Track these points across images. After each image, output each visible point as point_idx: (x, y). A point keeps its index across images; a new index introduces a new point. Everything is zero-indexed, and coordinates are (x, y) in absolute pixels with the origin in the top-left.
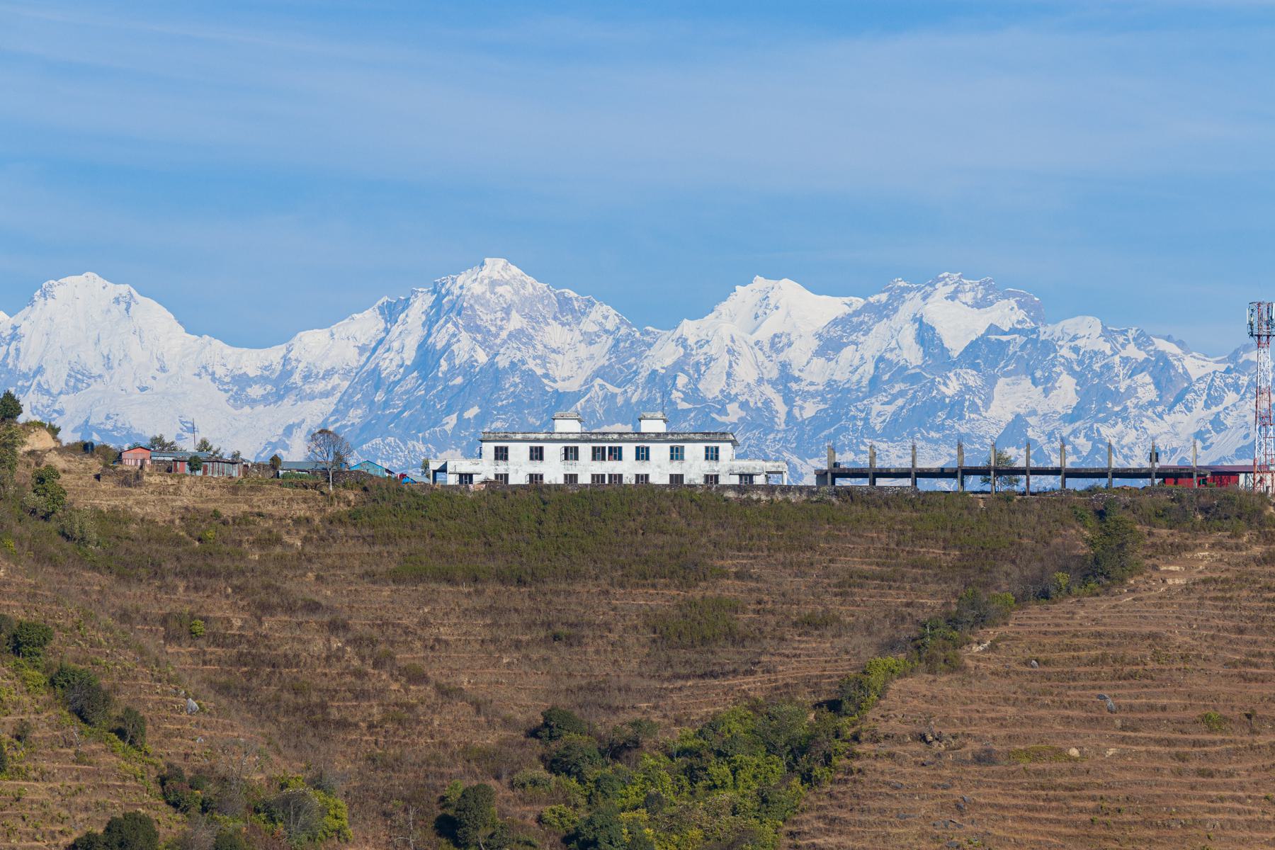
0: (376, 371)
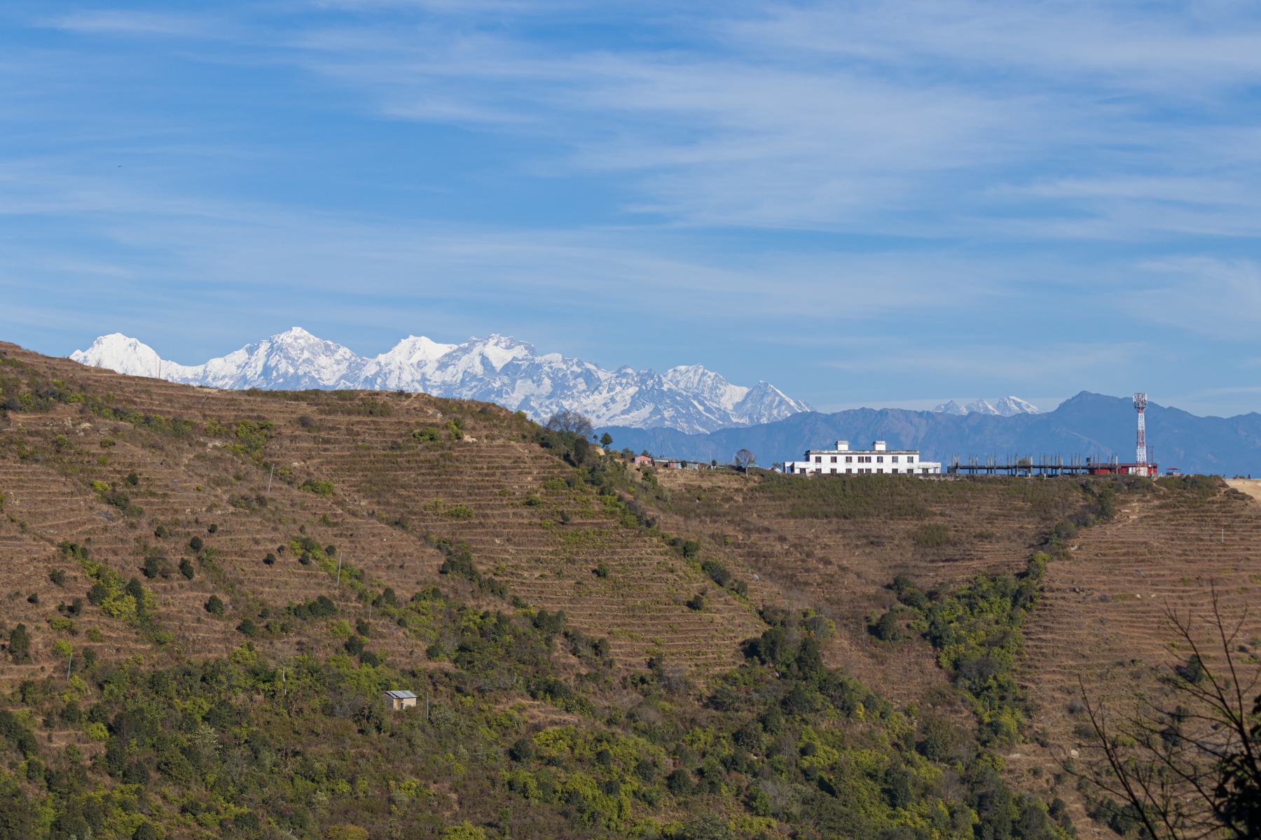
0: (244, 377)
